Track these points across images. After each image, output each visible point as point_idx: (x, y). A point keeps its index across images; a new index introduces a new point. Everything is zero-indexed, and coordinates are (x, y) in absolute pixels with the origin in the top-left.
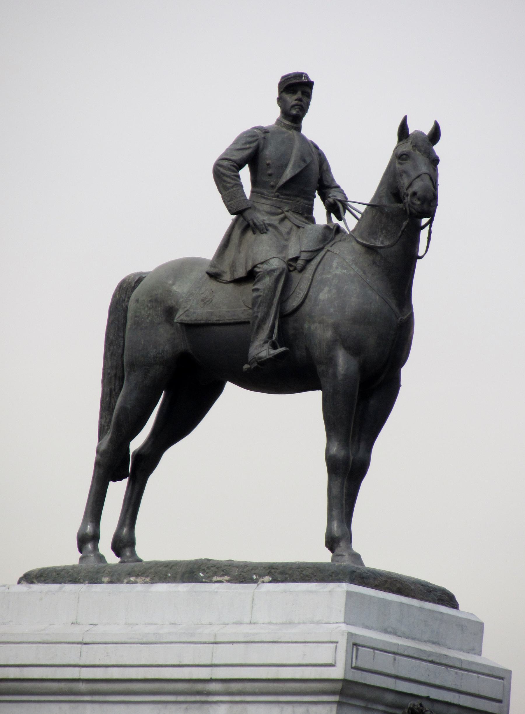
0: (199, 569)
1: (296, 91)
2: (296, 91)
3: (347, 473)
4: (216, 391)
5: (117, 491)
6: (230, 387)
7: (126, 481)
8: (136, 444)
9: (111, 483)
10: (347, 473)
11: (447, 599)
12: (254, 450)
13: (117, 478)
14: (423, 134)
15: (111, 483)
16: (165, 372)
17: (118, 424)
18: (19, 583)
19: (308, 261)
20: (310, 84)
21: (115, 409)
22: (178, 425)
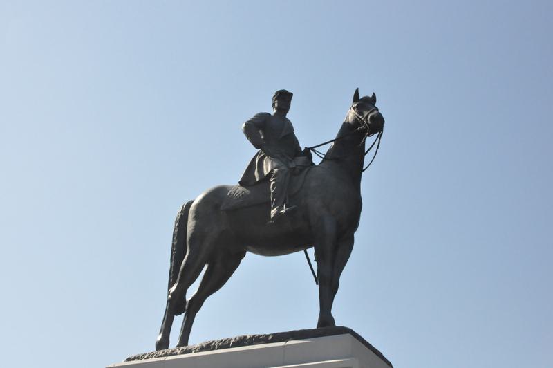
0: (254, 341)
1: (284, 99)
2: (284, 99)
3: (328, 285)
4: (243, 255)
5: (179, 320)
6: (247, 252)
7: (183, 314)
8: (192, 292)
9: (175, 316)
10: (328, 285)
11: (390, 364)
12: (269, 291)
13: (179, 313)
14: (369, 97)
15: (175, 316)
16: (212, 243)
17: (180, 275)
18: (374, 94)
19: (301, 171)
20: (290, 95)
21: (180, 271)
22: (212, 285)
